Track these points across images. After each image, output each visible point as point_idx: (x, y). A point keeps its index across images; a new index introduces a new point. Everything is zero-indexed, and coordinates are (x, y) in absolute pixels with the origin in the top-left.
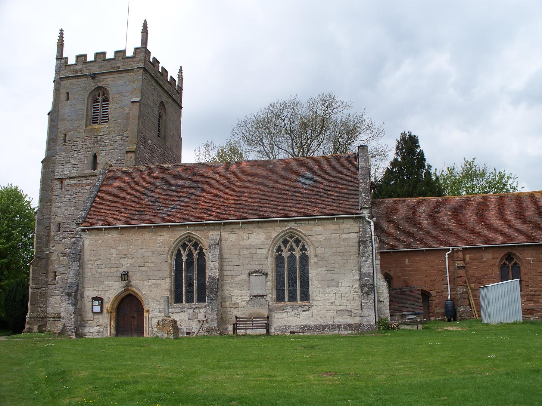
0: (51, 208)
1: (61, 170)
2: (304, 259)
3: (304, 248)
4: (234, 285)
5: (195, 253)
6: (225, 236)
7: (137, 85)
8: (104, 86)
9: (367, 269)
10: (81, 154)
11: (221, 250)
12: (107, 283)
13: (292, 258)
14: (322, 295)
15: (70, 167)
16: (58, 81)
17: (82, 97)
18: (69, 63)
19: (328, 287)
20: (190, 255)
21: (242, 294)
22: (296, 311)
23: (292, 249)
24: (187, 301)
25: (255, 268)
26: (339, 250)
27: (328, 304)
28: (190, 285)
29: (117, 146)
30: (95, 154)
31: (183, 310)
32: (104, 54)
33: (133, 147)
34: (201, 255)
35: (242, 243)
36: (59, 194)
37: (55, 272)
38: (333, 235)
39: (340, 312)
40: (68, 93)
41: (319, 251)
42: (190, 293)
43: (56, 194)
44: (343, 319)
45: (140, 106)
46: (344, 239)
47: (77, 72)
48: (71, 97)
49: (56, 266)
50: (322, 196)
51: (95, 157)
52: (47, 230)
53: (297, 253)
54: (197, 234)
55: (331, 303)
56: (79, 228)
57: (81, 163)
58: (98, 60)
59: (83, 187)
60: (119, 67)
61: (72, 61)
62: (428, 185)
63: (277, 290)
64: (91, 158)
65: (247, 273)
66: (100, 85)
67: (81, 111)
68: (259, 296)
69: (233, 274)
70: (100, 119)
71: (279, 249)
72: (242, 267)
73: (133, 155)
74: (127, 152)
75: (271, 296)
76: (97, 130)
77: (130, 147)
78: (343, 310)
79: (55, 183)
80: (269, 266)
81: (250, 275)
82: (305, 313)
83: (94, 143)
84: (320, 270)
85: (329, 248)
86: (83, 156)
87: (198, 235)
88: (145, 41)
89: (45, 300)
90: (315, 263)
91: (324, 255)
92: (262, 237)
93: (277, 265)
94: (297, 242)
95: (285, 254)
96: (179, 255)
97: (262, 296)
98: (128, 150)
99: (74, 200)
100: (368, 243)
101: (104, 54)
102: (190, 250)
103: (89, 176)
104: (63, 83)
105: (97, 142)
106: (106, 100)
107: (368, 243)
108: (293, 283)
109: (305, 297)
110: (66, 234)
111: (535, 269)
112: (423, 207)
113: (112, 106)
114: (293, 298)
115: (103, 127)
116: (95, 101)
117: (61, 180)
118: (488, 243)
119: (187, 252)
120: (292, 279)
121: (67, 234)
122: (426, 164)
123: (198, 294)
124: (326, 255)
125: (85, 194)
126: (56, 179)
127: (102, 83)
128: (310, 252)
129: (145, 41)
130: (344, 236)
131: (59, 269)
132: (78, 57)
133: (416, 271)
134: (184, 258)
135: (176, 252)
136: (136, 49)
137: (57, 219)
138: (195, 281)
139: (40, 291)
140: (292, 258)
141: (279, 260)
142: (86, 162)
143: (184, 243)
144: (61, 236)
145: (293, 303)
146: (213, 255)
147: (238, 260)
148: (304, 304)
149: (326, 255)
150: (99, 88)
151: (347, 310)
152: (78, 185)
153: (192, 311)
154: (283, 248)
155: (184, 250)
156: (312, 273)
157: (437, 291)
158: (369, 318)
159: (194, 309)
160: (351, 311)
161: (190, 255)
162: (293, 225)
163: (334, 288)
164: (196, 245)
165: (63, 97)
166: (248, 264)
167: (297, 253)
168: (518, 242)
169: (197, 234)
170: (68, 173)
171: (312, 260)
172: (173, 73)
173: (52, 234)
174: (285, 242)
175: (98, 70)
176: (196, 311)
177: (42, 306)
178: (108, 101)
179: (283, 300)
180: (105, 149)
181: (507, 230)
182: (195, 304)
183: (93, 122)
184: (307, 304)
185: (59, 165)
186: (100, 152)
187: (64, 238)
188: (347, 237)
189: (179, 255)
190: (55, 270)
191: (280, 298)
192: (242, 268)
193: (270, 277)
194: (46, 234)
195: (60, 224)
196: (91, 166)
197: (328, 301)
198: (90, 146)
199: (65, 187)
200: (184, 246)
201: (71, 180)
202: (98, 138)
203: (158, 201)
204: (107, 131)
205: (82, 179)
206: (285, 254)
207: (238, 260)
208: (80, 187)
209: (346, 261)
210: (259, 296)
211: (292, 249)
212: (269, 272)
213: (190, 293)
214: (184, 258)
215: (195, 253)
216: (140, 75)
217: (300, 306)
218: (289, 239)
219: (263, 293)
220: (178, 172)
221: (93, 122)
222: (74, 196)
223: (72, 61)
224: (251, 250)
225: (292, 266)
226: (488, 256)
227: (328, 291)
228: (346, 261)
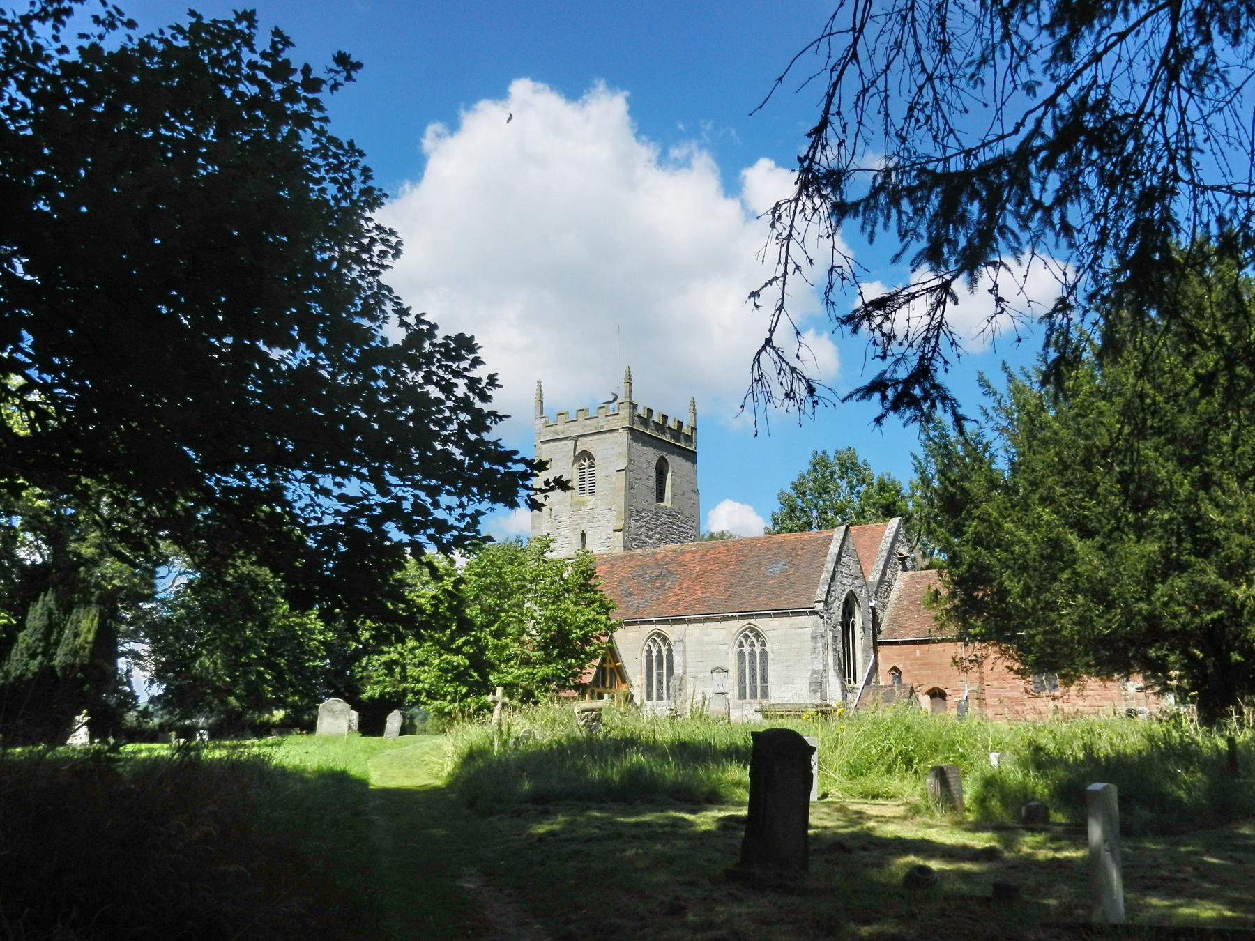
2: (764, 654)
3: (764, 644)
5: (664, 649)
7: (624, 449)
11: (684, 647)
13: (753, 653)
20: (660, 652)
23: (752, 645)
25: (718, 665)
33: (620, 525)
34: (670, 651)
35: (706, 639)
42: (754, 689)
45: (626, 475)
46: (799, 634)
51: (583, 535)
53: (758, 649)
58: (580, 419)
60: (602, 427)
62: (1047, 442)
70: (587, 491)
71: (741, 645)
73: (620, 534)
75: (733, 693)
76: (583, 503)
80: (732, 663)
83: (582, 519)
87: (830, 567)
90: (773, 660)
92: (723, 632)
95: (747, 650)
96: (649, 652)
106: (592, 466)
132: (792, 488)
134: (654, 654)
135: (646, 648)
140: (753, 653)
141: (741, 655)
154: (744, 643)
156: (771, 669)
161: (660, 652)
167: (758, 649)
169: (671, 631)
171: (770, 656)
179: (745, 698)
206: (747, 650)
211: (752, 645)
212: (730, 669)
213: (754, 689)
214: (654, 654)
215: (664, 649)
227: (785, 688)
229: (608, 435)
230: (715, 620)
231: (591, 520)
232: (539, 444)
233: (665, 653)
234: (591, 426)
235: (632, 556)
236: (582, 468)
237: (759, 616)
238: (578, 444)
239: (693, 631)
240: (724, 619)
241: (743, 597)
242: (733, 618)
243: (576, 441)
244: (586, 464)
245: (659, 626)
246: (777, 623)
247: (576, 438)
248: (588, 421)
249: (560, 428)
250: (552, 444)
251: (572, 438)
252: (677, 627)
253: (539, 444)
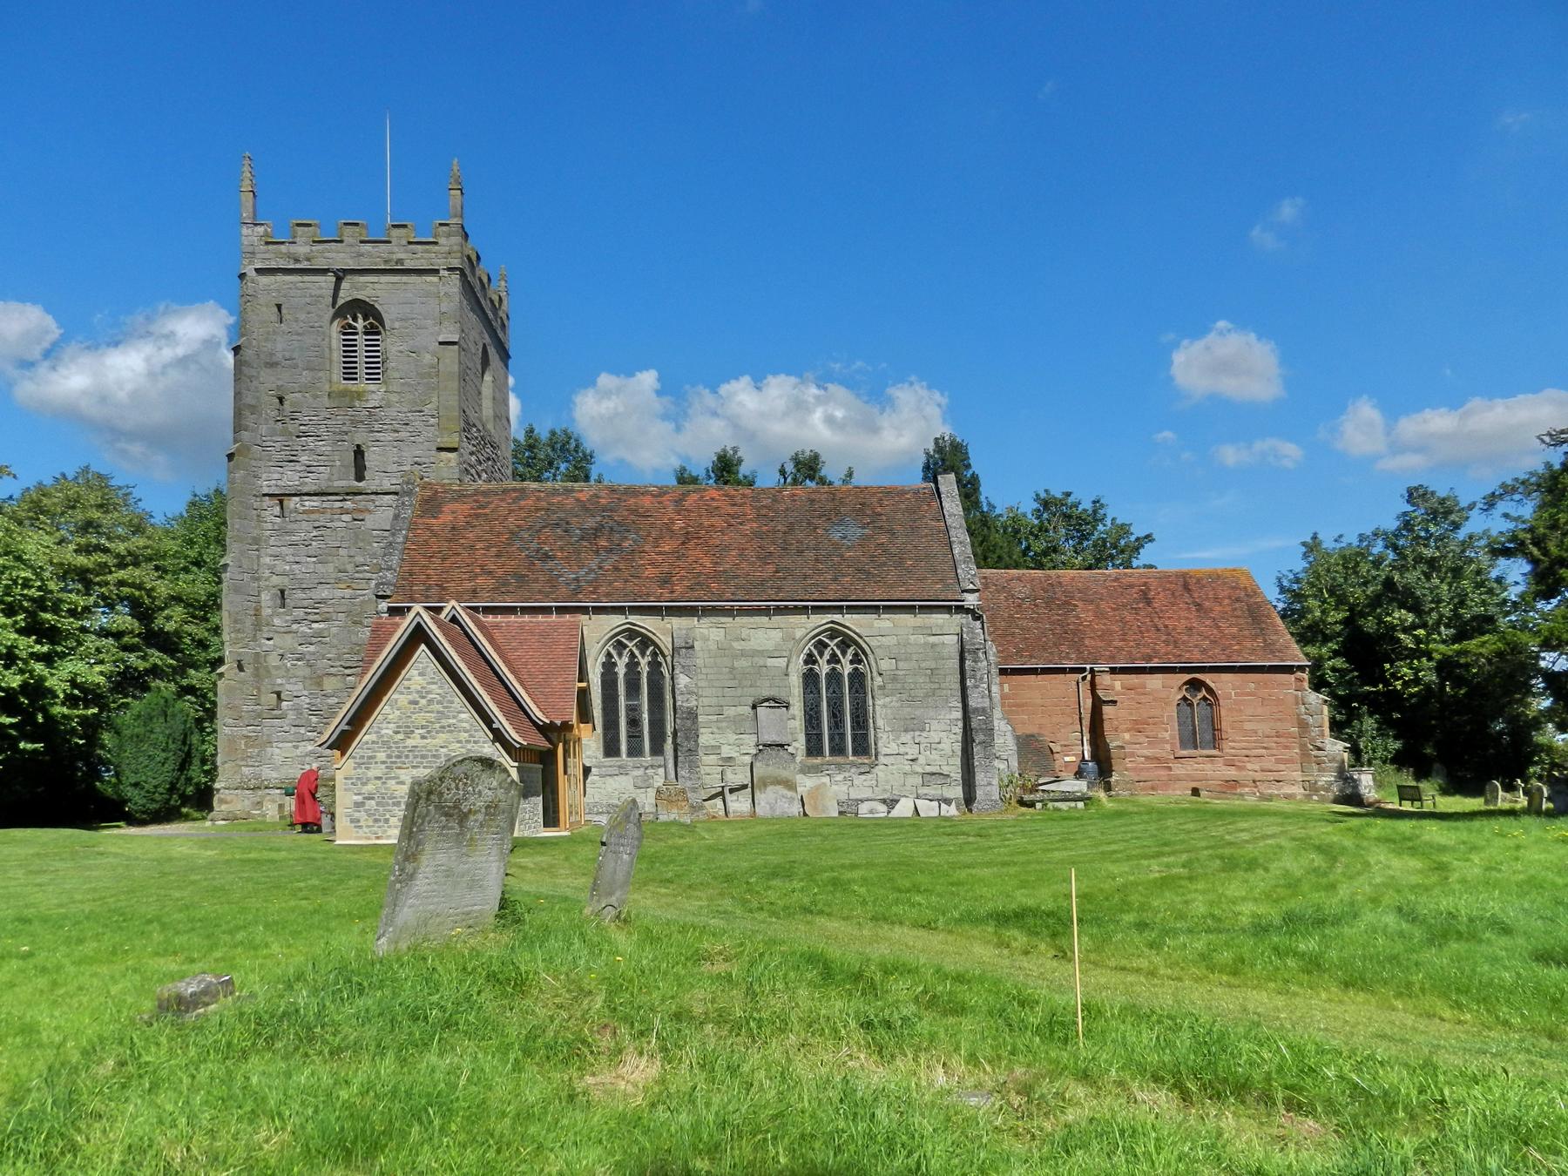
0: (259, 557)
1: (276, 476)
2: (858, 679)
4: (724, 724)
5: (644, 663)
8: (367, 300)
9: (980, 700)
10: (324, 445)
13: (834, 677)
14: (893, 745)
15: (300, 472)
17: (316, 319)
19: (906, 731)
21: (741, 742)
22: (847, 774)
24: (630, 754)
25: (766, 693)
26: (923, 665)
27: (906, 762)
28: (634, 722)
29: (409, 434)
30: (358, 446)
31: (623, 771)
36: (276, 528)
37: (279, 694)
38: (912, 637)
39: (927, 778)
40: (279, 307)
42: (635, 737)
43: (270, 526)
44: (936, 789)
46: (933, 645)
47: (297, 261)
48: (288, 317)
49: (279, 681)
50: (884, 564)
51: (359, 453)
52: (254, 605)
54: (658, 628)
55: (912, 760)
56: (384, 605)
57: (326, 463)
59: (336, 517)
60: (400, 261)
63: (807, 734)
65: (750, 701)
66: (359, 297)
67: (317, 349)
68: (777, 745)
69: (722, 703)
72: (739, 690)
74: (440, 449)
75: (799, 745)
76: (359, 395)
77: (445, 439)
78: (934, 774)
79: (264, 504)
81: (754, 707)
82: (863, 777)
83: (354, 423)
84: (888, 699)
85: (906, 660)
86: (329, 448)
89: (256, 750)
91: (896, 672)
93: (805, 689)
95: (823, 668)
97: (782, 746)
98: (442, 446)
99: (314, 543)
100: (980, 655)
102: (633, 655)
103: (347, 494)
105: (362, 422)
107: (980, 655)
108: (836, 723)
109: (862, 747)
110: (300, 613)
111: (1241, 710)
112: (1021, 590)
113: (391, 344)
114: (838, 749)
118: (1156, 660)
119: (626, 659)
120: (834, 715)
121: (302, 614)
122: (982, 498)
123: (652, 739)
124: (901, 673)
125: (341, 531)
126: (265, 495)
127: (363, 292)
130: (932, 639)
131: (288, 687)
133: (1022, 705)
134: (621, 670)
137: (275, 580)
138: (646, 716)
139: (245, 733)
140: (834, 677)
141: (810, 679)
142: (338, 463)
143: (619, 642)
144: (288, 618)
145: (839, 759)
146: (683, 667)
147: (732, 676)
148: (860, 761)
149: (901, 673)
151: (942, 774)
152: (323, 511)
153: (640, 772)
155: (620, 655)
157: (1063, 743)
158: (989, 788)
159: (646, 768)
160: (948, 776)
161: (633, 665)
163: (917, 733)
166: (751, 686)
168: (1210, 660)
169: (658, 628)
170: (297, 483)
173: (266, 612)
174: (821, 646)
175: (351, 262)
176: (650, 771)
177: (250, 763)
178: (378, 333)
180: (382, 439)
181: (1185, 638)
182: (648, 759)
183: (346, 376)
184: (866, 761)
185: (271, 464)
186: (370, 444)
187: (296, 621)
188: (937, 642)
190: (278, 689)
191: (814, 749)
192: (739, 692)
194: (252, 613)
195: (282, 592)
196: (352, 476)
197: (906, 757)
198: (345, 428)
199: (291, 512)
201: (306, 498)
202: (362, 414)
203: (553, 558)
204: (383, 399)
205: (330, 498)
206: (823, 668)
207: (732, 676)
208: (329, 516)
209: (937, 686)
210: (777, 745)
213: (635, 737)
214: (621, 670)
215: (644, 663)
216: (453, 284)
217: (853, 764)
218: (827, 641)
220: (578, 500)
221: (346, 376)
222: (315, 534)
224: (756, 659)
225: (834, 692)
226: (1155, 682)
227: (906, 738)
228: (937, 686)
229: (413, 279)
230: (765, 612)
231: (377, 427)
232: (252, 273)
233: (644, 669)
234: (374, 256)
235: (523, 490)
236: (348, 330)
237: (851, 610)
238: (345, 285)
239: (707, 632)
240: (780, 611)
241: (805, 577)
242: (804, 610)
243: (339, 280)
244: (360, 324)
245: (633, 619)
246: (888, 624)
247: (341, 275)
248: (368, 247)
249: (301, 249)
250: (280, 278)
251: (335, 272)
252: (677, 623)
253: (252, 273)
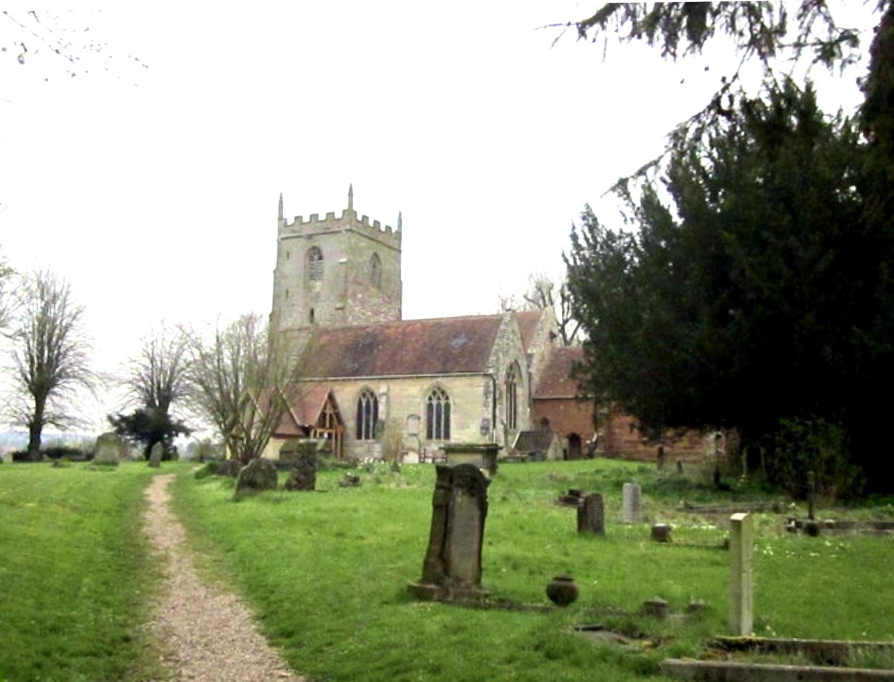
2: (447, 406)
3: (447, 398)
5: (372, 401)
6: (381, 388)
12: (58, 498)
13: (439, 405)
16: (281, 241)
18: (289, 223)
23: (439, 399)
25: (413, 413)
28: (368, 425)
32: (317, 215)
34: (376, 403)
41: (457, 400)
51: (312, 312)
53: (443, 402)
54: (372, 385)
61: (290, 221)
64: (308, 313)
71: (430, 399)
75: (423, 434)
80: (422, 411)
88: (351, 204)
94: (443, 392)
95: (435, 402)
101: (317, 215)
104: (285, 242)
106: (321, 258)
115: (318, 285)
116: (311, 259)
117: (285, 332)
128: (451, 401)
129: (351, 204)
132: (296, 218)
134: (364, 404)
135: (357, 399)
136: (344, 211)
140: (439, 405)
141: (430, 406)
150: (314, 248)
156: (452, 417)
161: (368, 403)
162: (439, 380)
164: (372, 394)
165: (284, 255)
167: (443, 402)
169: (372, 385)
171: (452, 407)
172: (666, 207)
174: (434, 393)
189: (360, 403)
193: (422, 420)
200: (364, 395)
206: (435, 402)
211: (439, 399)
214: (364, 404)
215: (372, 401)
219: (416, 432)
223: (290, 221)
227: (462, 432)
